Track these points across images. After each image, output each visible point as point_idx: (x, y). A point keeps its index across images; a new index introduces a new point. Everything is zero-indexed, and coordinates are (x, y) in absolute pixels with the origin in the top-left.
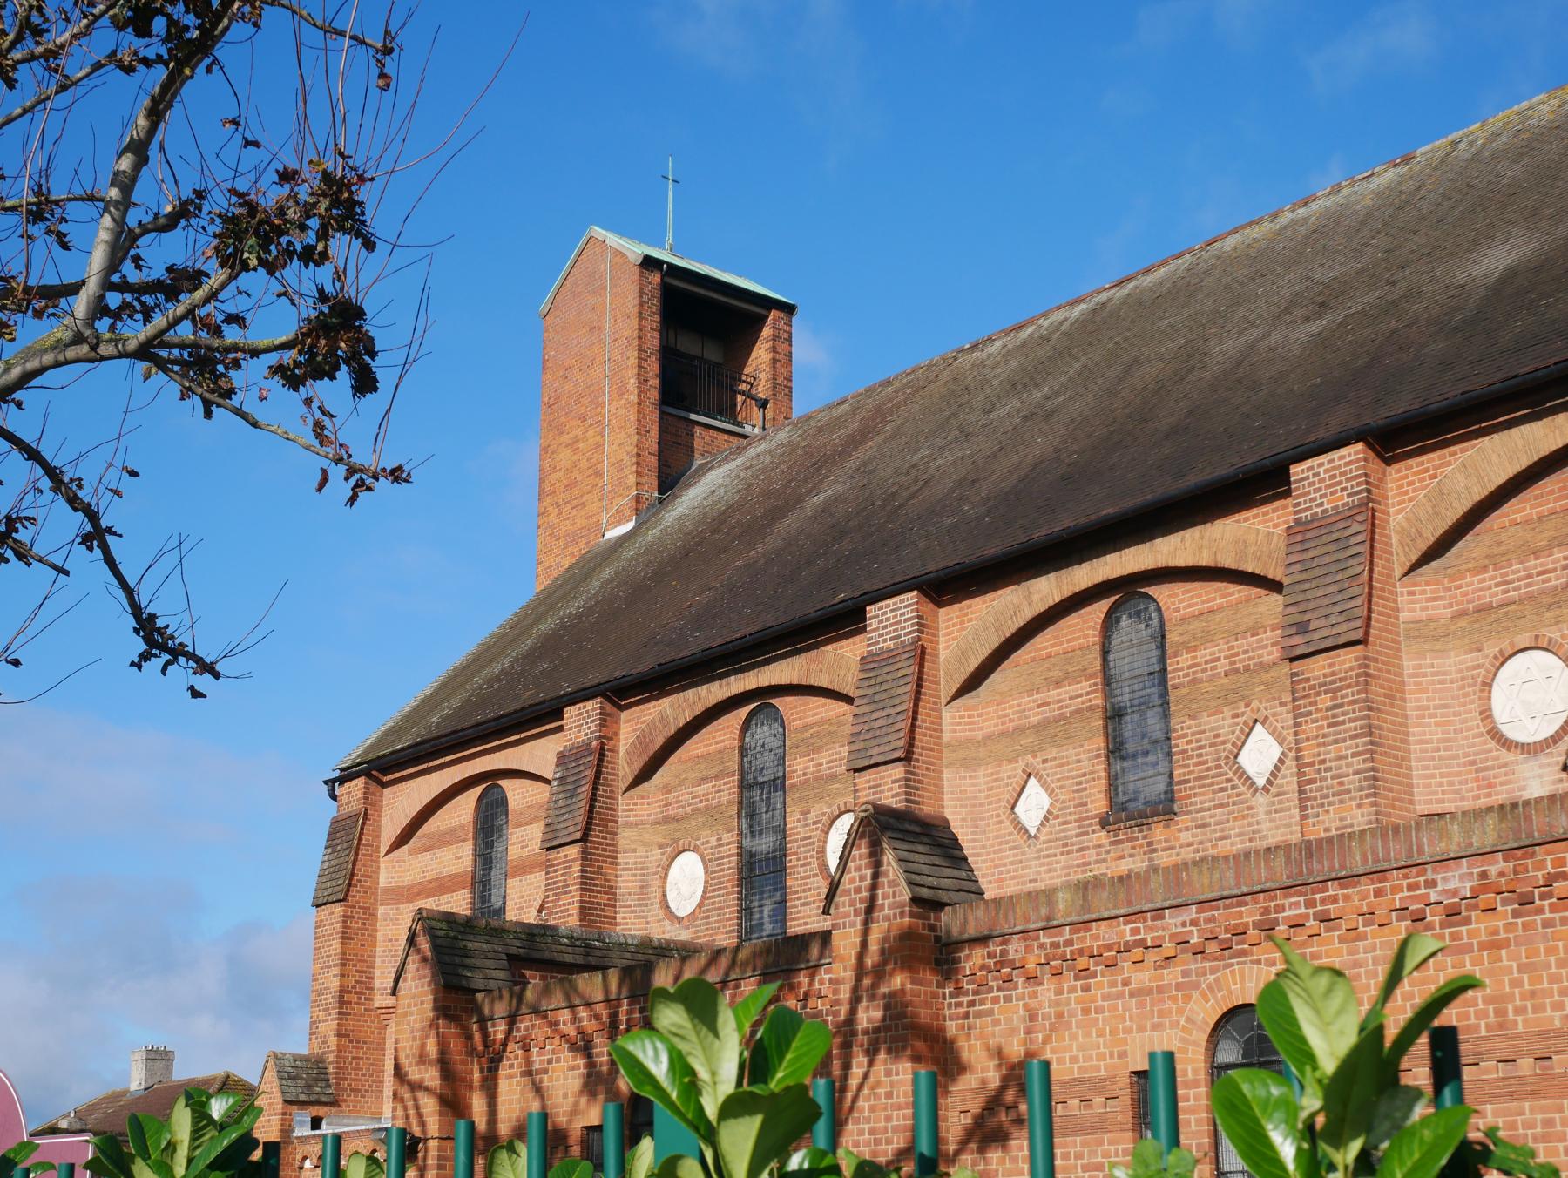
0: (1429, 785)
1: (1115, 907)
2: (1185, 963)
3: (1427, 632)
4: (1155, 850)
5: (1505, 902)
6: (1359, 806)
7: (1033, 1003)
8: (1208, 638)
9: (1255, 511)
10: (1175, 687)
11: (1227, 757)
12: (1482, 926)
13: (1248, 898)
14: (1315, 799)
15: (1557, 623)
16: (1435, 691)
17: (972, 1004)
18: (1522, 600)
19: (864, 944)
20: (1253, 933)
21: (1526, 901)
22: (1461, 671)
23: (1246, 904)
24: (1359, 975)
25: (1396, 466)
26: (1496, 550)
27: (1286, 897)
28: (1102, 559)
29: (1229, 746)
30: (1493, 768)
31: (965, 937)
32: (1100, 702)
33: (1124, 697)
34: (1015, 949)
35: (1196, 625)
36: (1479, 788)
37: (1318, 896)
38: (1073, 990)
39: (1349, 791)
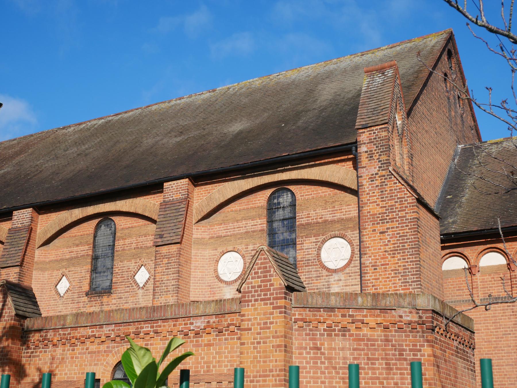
0: (195, 292)
1: (87, 323)
6: (172, 296)
7: (54, 354)
8: (130, 236)
9: (151, 196)
10: (117, 251)
11: (131, 276)
13: (132, 324)
16: (201, 261)
17: (32, 352)
18: (231, 236)
22: (210, 256)
23: (131, 325)
25: (198, 188)
26: (225, 219)
27: (144, 324)
29: (132, 272)
30: (215, 288)
31: (33, 329)
32: (91, 253)
33: (99, 253)
34: (50, 334)
35: (127, 231)
36: (210, 294)
37: (155, 325)
38: (68, 350)
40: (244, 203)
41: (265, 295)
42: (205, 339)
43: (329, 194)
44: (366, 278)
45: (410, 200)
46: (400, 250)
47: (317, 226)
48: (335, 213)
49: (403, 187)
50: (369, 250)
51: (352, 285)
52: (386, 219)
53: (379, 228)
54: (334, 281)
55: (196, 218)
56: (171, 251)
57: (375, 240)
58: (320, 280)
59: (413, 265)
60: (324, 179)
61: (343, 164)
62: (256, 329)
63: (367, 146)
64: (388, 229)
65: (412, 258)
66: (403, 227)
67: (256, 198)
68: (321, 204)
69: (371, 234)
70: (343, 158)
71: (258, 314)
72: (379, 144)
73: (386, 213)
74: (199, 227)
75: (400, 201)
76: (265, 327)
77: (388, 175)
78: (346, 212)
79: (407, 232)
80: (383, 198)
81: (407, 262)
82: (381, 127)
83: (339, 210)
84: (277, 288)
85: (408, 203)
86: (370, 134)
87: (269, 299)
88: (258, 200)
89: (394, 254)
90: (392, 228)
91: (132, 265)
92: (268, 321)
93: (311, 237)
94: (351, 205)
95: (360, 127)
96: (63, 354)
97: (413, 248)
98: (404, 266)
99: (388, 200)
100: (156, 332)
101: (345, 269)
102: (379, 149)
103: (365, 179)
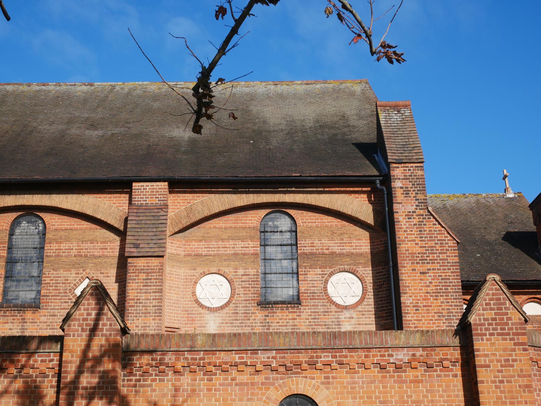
0: (170, 316)
1: (231, 346)
2: (266, 374)
3: (175, 258)
4: (26, 322)
5: (421, 366)
6: (154, 319)
7: (178, 383)
8: (67, 239)
9: (105, 195)
10: (47, 256)
11: (70, 290)
12: (411, 374)
13: (303, 351)
14: (133, 313)
15: (228, 266)
16: (176, 281)
17: (137, 380)
18: (214, 256)
19: (88, 347)
20: (305, 366)
21: (429, 367)
22: (186, 276)
23: (302, 353)
24: (355, 387)
25: (174, 195)
26: (206, 235)
27: (322, 352)
28: (22, 196)
29: (72, 285)
30: (195, 314)
31: (139, 349)
32: (5, 255)
34: (169, 358)
35: (63, 233)
36: (188, 320)
37: (338, 354)
38: (203, 380)
39: (150, 313)
40: (230, 220)
41: (501, 329)
42: (411, 374)
43: (336, 225)
44: (407, 318)
45: (451, 243)
46: (443, 292)
47: (323, 257)
48: (343, 246)
49: (443, 229)
50: (409, 290)
51: (366, 324)
52: (427, 260)
53: (420, 268)
54: (345, 318)
55: (171, 229)
56: (150, 264)
57: (415, 280)
58: (328, 315)
59: (457, 309)
60: (335, 208)
61: (357, 195)
62: (496, 366)
63: (402, 182)
64: (429, 269)
65: (456, 302)
66: (445, 269)
67: (247, 217)
68: (326, 234)
69: (411, 273)
70: (356, 189)
71: (496, 350)
72: (415, 182)
73: (426, 253)
74: (173, 240)
75: (441, 244)
76: (507, 364)
77: (426, 215)
78: (356, 246)
79: (449, 276)
80: (422, 237)
81: (452, 306)
82: (416, 165)
83: (349, 243)
84: (516, 323)
85: (449, 247)
86: (404, 170)
87: (508, 334)
88: (250, 220)
89: (436, 296)
90: (433, 269)
91: (72, 275)
92: (510, 358)
93: (316, 268)
94: (362, 240)
95: (394, 161)
96: (193, 385)
97: (456, 292)
98: (448, 309)
99: (428, 240)
100: (341, 364)
101: (357, 306)
102: (415, 187)
103: (401, 215)
